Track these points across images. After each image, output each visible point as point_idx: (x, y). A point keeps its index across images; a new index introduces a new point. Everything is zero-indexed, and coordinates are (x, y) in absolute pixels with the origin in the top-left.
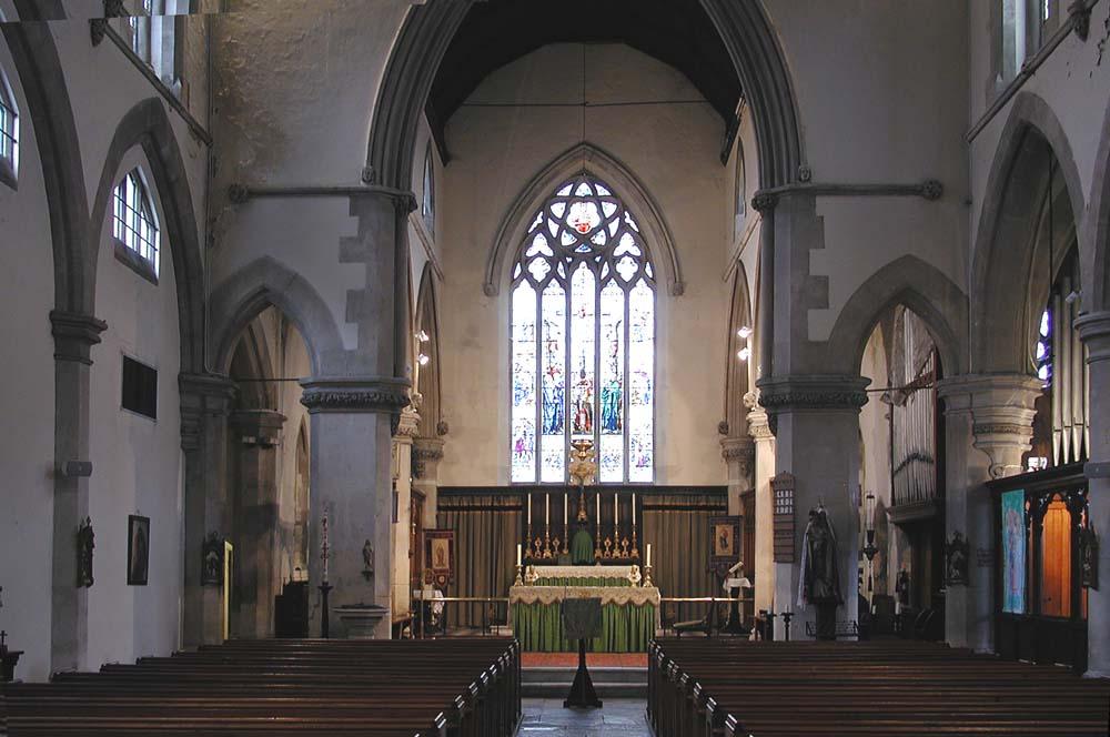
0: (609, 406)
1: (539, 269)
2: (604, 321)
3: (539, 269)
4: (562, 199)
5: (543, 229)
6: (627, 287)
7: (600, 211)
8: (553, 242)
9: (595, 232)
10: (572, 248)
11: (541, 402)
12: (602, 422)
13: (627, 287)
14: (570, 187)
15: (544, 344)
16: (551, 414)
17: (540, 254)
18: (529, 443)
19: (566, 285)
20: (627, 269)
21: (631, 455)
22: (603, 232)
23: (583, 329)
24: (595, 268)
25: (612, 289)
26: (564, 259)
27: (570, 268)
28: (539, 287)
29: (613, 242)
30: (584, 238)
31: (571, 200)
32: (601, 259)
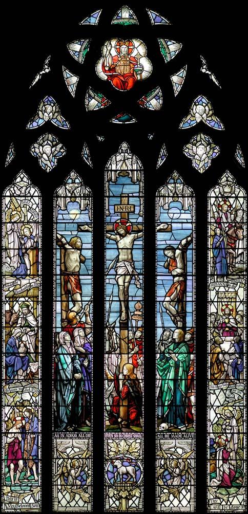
0: (171, 384)
1: (47, 153)
2: (162, 239)
3: (47, 153)
4: (143, 17)
5: (54, 85)
6: (201, 184)
7: (154, 54)
8: (71, 106)
9: (144, 87)
10: (102, 115)
11: (50, 379)
12: (159, 412)
13: (201, 184)
14: (177, 89)
15: (58, 279)
16: (69, 397)
17: (48, 127)
18: (33, 446)
19: (95, 182)
20: (201, 154)
21: (209, 468)
22: (158, 91)
23: (124, 248)
24: (145, 153)
25: (175, 186)
26: (87, 145)
27: (103, 154)
28: (48, 184)
29: (178, 106)
30: (124, 97)
31: (96, 40)
32: (161, 145)
